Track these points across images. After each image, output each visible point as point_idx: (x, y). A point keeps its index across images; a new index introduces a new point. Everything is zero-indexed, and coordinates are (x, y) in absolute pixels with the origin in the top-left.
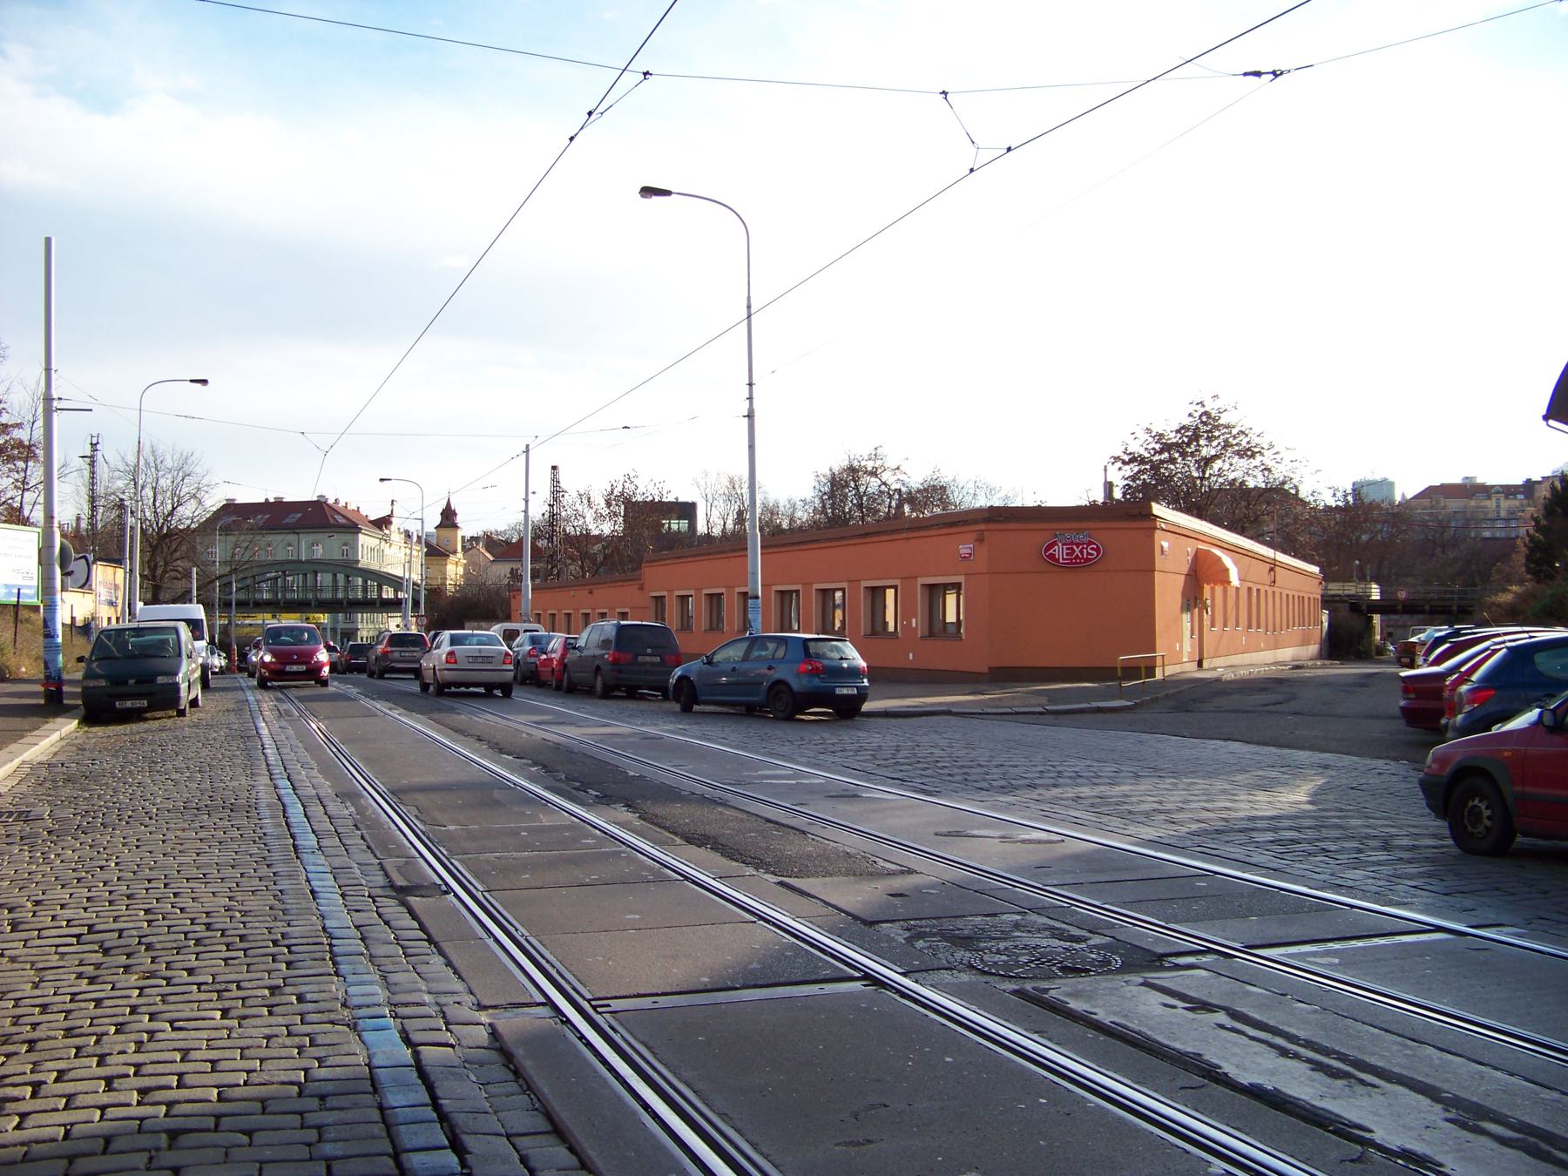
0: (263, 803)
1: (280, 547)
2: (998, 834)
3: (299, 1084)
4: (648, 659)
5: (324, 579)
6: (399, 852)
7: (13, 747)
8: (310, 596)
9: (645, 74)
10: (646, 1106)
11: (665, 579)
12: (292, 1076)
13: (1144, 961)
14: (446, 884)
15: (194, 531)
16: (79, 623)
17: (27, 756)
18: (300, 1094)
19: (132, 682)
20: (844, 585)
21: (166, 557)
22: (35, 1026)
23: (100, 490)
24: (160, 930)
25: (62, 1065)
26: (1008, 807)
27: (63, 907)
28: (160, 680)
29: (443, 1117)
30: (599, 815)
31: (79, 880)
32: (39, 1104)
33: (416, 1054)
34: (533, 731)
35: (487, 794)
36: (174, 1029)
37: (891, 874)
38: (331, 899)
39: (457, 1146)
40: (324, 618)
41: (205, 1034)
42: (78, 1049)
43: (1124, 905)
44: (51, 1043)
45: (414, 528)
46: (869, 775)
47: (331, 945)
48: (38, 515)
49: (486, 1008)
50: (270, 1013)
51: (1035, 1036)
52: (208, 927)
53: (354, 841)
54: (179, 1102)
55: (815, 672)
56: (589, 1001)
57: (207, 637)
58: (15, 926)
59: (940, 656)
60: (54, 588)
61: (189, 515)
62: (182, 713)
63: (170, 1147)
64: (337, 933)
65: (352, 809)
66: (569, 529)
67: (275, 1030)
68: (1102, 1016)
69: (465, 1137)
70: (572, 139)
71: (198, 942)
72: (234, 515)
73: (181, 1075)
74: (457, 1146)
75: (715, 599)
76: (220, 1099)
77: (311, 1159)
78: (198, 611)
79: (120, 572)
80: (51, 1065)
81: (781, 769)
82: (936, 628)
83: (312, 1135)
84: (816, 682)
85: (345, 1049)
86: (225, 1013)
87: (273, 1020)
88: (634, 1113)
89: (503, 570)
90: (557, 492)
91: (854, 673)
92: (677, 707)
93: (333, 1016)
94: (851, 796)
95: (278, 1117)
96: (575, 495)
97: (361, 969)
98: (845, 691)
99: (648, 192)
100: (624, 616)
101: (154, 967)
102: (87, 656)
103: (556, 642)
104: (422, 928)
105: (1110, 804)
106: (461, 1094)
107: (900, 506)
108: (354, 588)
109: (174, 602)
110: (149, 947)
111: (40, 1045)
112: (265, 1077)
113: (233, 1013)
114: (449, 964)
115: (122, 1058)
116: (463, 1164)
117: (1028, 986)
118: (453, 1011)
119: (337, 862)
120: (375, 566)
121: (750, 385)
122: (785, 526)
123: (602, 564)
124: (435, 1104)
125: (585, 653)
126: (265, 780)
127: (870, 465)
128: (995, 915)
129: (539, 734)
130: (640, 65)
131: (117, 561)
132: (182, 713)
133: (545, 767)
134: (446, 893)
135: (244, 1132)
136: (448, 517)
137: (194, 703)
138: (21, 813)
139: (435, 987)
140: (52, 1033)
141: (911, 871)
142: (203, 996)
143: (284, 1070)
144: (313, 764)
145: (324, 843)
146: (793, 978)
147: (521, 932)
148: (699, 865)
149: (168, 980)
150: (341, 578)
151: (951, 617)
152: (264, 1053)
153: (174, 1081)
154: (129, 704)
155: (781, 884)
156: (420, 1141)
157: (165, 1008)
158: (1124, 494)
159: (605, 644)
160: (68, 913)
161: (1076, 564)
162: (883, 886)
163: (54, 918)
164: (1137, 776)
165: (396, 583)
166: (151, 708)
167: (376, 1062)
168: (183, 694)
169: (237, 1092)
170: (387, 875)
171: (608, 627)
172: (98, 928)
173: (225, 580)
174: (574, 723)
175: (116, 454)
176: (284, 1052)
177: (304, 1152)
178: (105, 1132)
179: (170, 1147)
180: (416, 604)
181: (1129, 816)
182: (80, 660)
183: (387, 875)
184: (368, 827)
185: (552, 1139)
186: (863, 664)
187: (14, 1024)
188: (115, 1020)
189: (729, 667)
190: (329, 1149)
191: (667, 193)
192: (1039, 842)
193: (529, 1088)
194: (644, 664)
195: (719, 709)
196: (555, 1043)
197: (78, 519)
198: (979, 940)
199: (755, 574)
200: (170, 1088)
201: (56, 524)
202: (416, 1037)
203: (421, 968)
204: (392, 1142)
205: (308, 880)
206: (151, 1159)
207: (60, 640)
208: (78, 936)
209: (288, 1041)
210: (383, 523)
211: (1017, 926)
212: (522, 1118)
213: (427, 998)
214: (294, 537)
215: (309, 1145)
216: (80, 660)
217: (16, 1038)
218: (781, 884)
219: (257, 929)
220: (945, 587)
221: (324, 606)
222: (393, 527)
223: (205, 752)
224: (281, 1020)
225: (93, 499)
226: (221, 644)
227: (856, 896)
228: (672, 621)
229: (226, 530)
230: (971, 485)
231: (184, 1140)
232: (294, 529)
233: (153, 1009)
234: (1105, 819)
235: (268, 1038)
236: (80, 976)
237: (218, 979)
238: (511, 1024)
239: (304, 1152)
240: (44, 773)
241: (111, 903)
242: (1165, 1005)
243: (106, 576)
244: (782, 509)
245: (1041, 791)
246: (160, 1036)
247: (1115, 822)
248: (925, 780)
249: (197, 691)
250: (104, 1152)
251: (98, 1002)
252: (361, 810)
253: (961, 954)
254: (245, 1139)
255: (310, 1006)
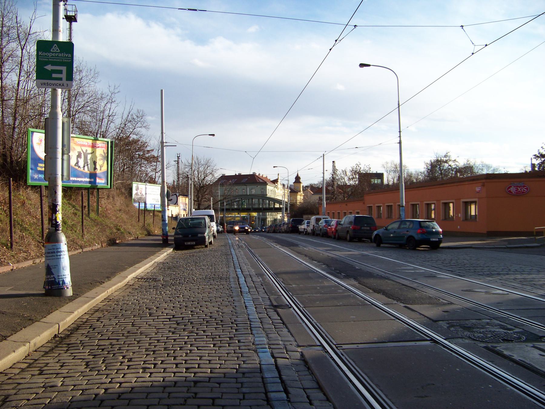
0: (231, 276)
1: (240, 190)
2: (484, 291)
3: (236, 369)
4: (365, 228)
5: (255, 201)
6: (276, 293)
7: (152, 257)
8: (250, 207)
9: (355, 26)
10: (351, 381)
11: (372, 200)
12: (234, 366)
13: (534, 338)
14: (291, 305)
15: (212, 185)
16: (174, 216)
17: (156, 260)
18: (236, 372)
19: (190, 236)
20: (435, 202)
21: (202, 193)
22: (155, 346)
23: (180, 172)
24: (195, 318)
25: (163, 359)
26: (489, 282)
27: (165, 309)
28: (199, 235)
29: (283, 382)
30: (345, 282)
31: (170, 301)
32: (155, 370)
33: (276, 361)
34: (324, 253)
35: (307, 274)
36: (198, 350)
37: (444, 304)
38: (252, 309)
39: (286, 391)
40: (255, 214)
41: (207, 352)
42: (168, 354)
43: (528, 318)
44: (160, 352)
45: (286, 183)
46: (440, 269)
47: (250, 324)
48: (160, 180)
49: (300, 346)
50: (229, 346)
51: (490, 363)
52: (211, 317)
53: (261, 290)
54: (198, 373)
55: (423, 233)
56: (335, 345)
57: (215, 221)
58: (150, 315)
59: (471, 228)
60: (165, 205)
61: (209, 179)
62: (206, 246)
63: (194, 386)
64: (252, 320)
65: (261, 279)
66: (339, 183)
67: (230, 351)
68: (516, 357)
69: (289, 389)
70: (330, 50)
71: (207, 322)
72: (224, 179)
73: (199, 364)
74: (286, 391)
75: (390, 207)
76: (211, 372)
77: (238, 393)
78: (212, 212)
79: (187, 199)
80: (159, 359)
81: (410, 267)
82: (467, 217)
83: (239, 385)
84: (424, 236)
85: (253, 358)
86: (214, 345)
87: (230, 348)
88: (347, 383)
89: (317, 197)
90: (334, 170)
91: (437, 233)
92: (375, 245)
93: (249, 347)
94: (432, 276)
95: (229, 379)
96: (341, 171)
97: (259, 332)
98: (434, 240)
99: (362, 65)
100: (358, 213)
101: (193, 329)
102: (176, 227)
103: (334, 222)
104: (281, 319)
105: (527, 281)
106: (289, 375)
107: (456, 173)
108: (266, 204)
109: (205, 209)
110: (191, 323)
111: (157, 352)
112: (226, 366)
113: (217, 345)
114: (289, 331)
115: (181, 358)
116: (288, 397)
117: (490, 345)
118: (289, 347)
119: (255, 297)
120: (272, 196)
121: (400, 132)
122: (415, 181)
123: (351, 195)
124: (280, 378)
125: (344, 226)
126: (232, 269)
127: (445, 159)
128: (480, 320)
129: (326, 254)
130: (353, 23)
131: (187, 196)
132: (206, 246)
133: (327, 265)
134: (290, 308)
135: (218, 383)
136: (298, 179)
137: (211, 243)
138: (154, 279)
139: (283, 339)
140: (160, 349)
141: (452, 303)
142: (208, 339)
143: (231, 365)
144: (249, 264)
145: (251, 290)
146: (406, 339)
147: (314, 321)
148: (378, 300)
149: (197, 334)
150: (261, 200)
151: (473, 213)
152: (226, 358)
153: (197, 366)
154: (189, 243)
155: (405, 307)
156: (273, 389)
157: (195, 343)
158: (539, 169)
159: (350, 223)
160: (167, 311)
161: (519, 194)
162: (441, 309)
163: (162, 312)
164: (539, 271)
165: (280, 202)
166: (196, 245)
167: (262, 363)
168: (207, 240)
169: (216, 371)
170: (271, 301)
171: (351, 217)
172: (176, 316)
173: (222, 202)
174: (339, 250)
175: (185, 160)
176: (232, 359)
177: (236, 391)
178: (175, 380)
179: (194, 386)
180: (286, 209)
181: (534, 286)
182: (173, 228)
183: (271, 301)
184: (265, 285)
185: (318, 390)
186: (441, 230)
187: (149, 345)
188: (180, 346)
189: (393, 231)
190: (244, 390)
191: (369, 65)
192: (499, 294)
193: (312, 373)
194: (364, 230)
195: (392, 246)
196: (323, 361)
197: (174, 182)
198: (473, 328)
199: (402, 198)
200: (195, 368)
201: (165, 184)
202: (276, 355)
203: (279, 333)
204: (265, 389)
205: (244, 303)
206: (188, 390)
207: (167, 222)
208: (169, 319)
209: (234, 355)
210: (275, 182)
211: (488, 324)
212: (308, 383)
213: (281, 342)
214: (245, 187)
215: (238, 388)
216: (173, 228)
217: (150, 350)
218: (405, 307)
219: (227, 318)
220: (471, 202)
221: (255, 210)
222: (279, 183)
223: (213, 259)
224: (232, 348)
225: (178, 174)
226: (221, 223)
227: (432, 312)
228: (375, 215)
229: (222, 185)
230: (481, 166)
231: (198, 385)
232: (245, 184)
233: (191, 343)
234: (525, 287)
235: (228, 354)
236: (170, 331)
237: (213, 334)
238: (309, 353)
239: (236, 391)
240: (161, 266)
241: (180, 308)
242: (541, 355)
243: (182, 200)
244: (413, 175)
245: (502, 276)
246: (193, 351)
247: (529, 288)
248: (460, 271)
249: (212, 239)
250: (174, 386)
251: (175, 340)
252: (264, 280)
253: (467, 333)
254: (218, 385)
255: (242, 344)
